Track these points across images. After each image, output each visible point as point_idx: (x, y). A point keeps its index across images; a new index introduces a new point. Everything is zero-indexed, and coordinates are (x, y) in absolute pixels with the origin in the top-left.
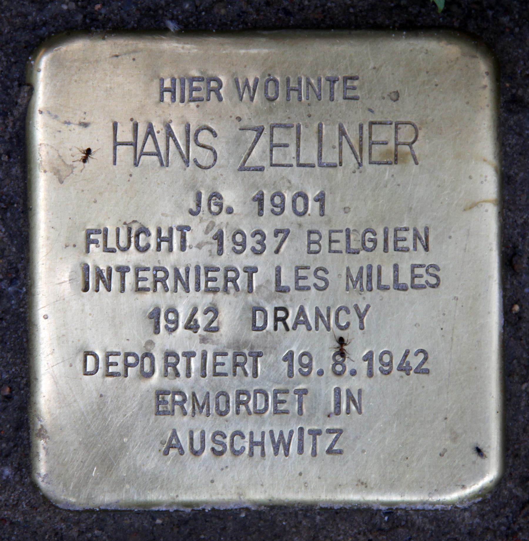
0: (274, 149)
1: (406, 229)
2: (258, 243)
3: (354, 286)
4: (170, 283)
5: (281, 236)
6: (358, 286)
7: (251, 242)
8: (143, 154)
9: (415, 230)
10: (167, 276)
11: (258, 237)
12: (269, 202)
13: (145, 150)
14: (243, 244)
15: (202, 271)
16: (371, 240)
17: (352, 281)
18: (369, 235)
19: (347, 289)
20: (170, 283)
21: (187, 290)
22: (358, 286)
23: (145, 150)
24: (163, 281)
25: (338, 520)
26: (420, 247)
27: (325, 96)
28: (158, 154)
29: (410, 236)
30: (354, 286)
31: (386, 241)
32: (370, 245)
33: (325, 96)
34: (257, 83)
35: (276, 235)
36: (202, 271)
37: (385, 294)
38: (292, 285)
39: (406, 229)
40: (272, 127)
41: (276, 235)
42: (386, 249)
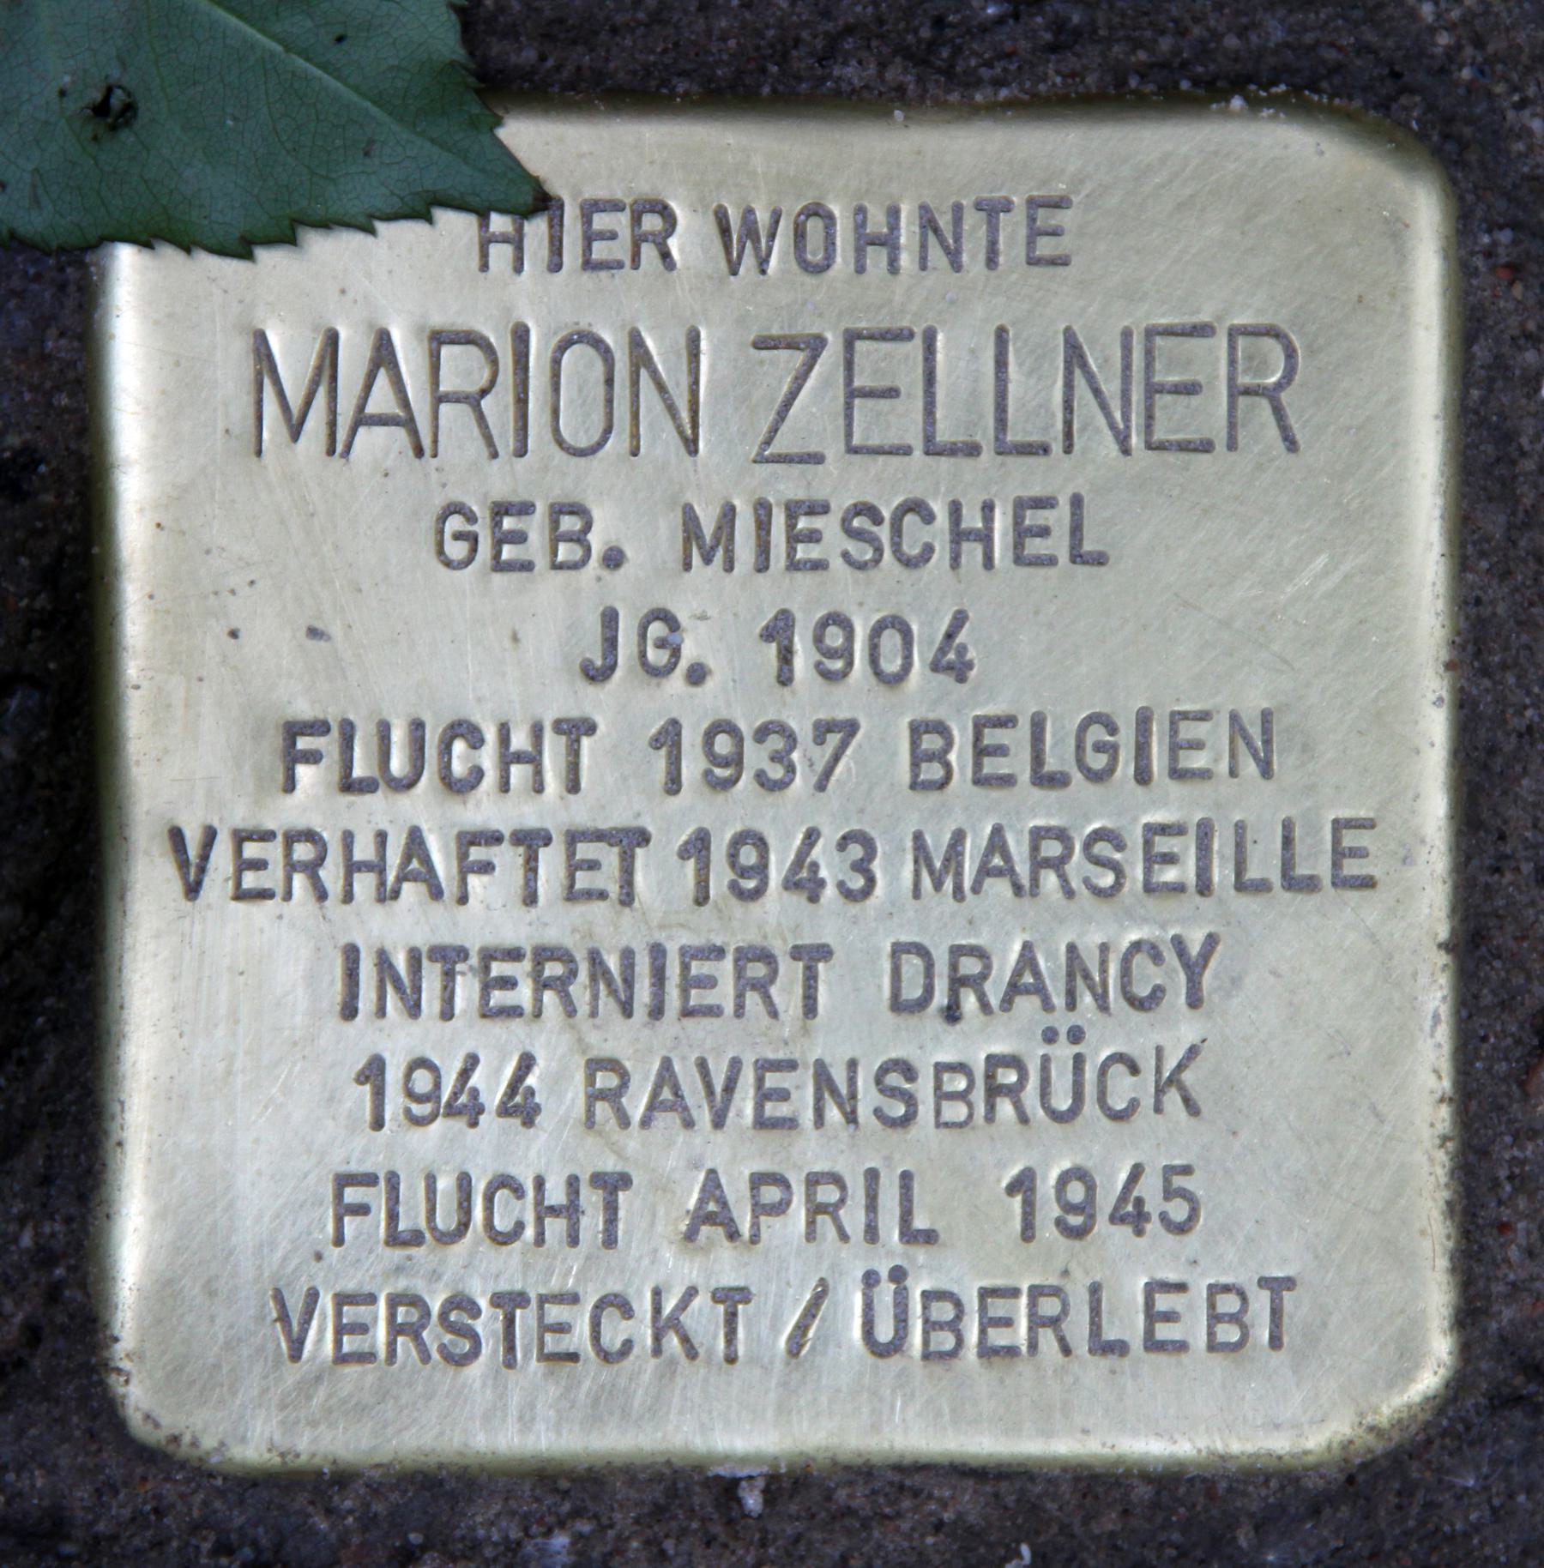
0: (857, 401)
1: (1204, 716)
2: (776, 758)
3: (938, 885)
4: (331, 874)
5: (834, 739)
6: (949, 885)
7: (755, 757)
8: (362, 419)
9: (1234, 718)
10: (320, 860)
11: (776, 742)
12: (699, 750)
13: (371, 408)
14: (736, 761)
15: (779, 520)
16: (1099, 747)
17: (931, 872)
18: (1096, 733)
19: (917, 892)
20: (331, 874)
21: (414, 1010)
22: (949, 885)
23: (371, 408)
24: (312, 869)
25: (899, 1393)
26: (1250, 768)
27: (974, 256)
28: (409, 423)
29: (1217, 734)
30: (938, 885)
31: (1142, 749)
32: (1098, 762)
33: (974, 256)
34: (777, 222)
35: (819, 740)
36: (779, 520)
37: (1310, 902)
38: (1324, 869)
39: (1204, 716)
40: (851, 338)
41: (819, 740)
42: (1143, 776)
